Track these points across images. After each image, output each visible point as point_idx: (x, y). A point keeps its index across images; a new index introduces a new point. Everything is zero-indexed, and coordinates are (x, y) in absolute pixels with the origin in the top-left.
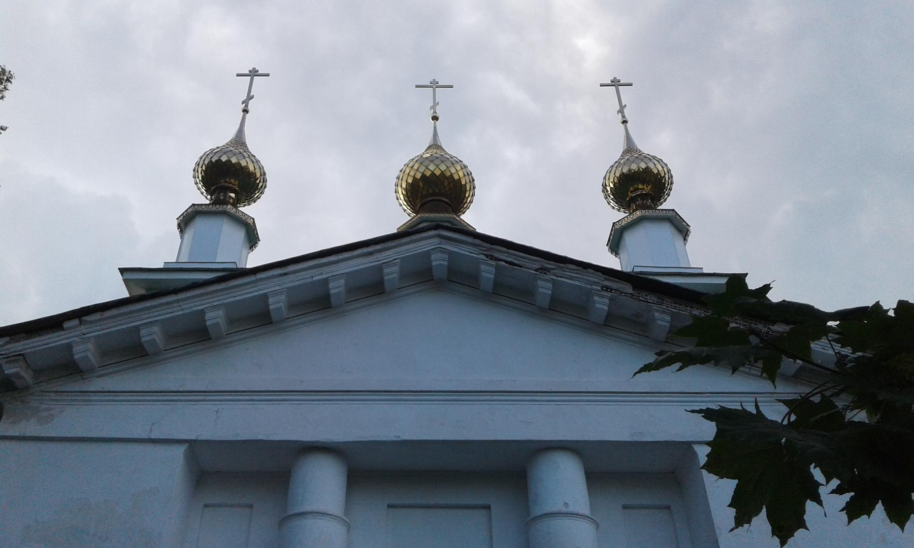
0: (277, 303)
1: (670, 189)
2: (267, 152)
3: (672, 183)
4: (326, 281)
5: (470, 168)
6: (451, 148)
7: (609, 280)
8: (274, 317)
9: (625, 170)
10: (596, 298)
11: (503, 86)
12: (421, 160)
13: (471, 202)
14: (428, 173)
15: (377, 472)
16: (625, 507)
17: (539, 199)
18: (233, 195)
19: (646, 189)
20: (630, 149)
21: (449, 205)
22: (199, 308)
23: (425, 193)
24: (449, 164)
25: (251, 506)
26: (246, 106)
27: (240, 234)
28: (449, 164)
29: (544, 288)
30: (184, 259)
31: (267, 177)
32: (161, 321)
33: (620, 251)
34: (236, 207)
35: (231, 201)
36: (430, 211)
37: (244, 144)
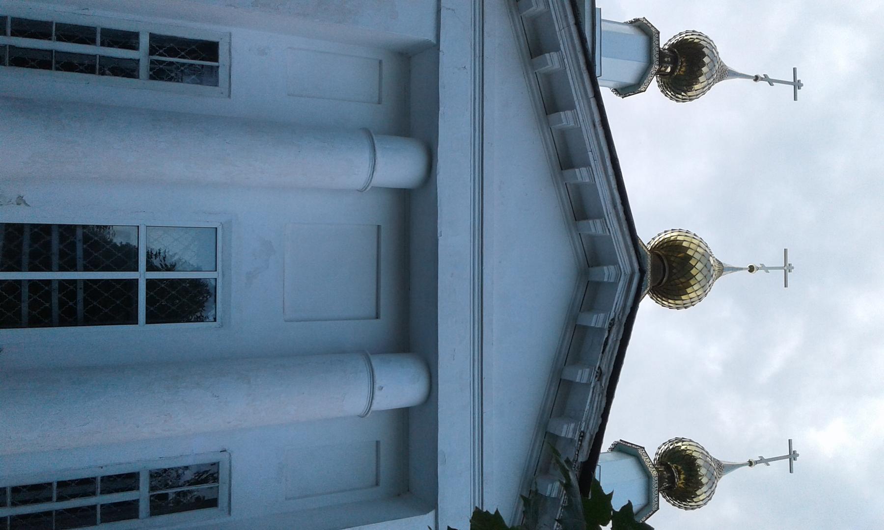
0: (566, 119)
1: (679, 507)
2: (713, 102)
3: (686, 509)
4: (587, 164)
5: (698, 305)
6: (719, 285)
7: (591, 439)
8: (553, 116)
9: (699, 462)
10: (572, 425)
11: (785, 346)
12: (706, 255)
13: (663, 305)
14: (692, 262)
15: (409, 216)
16: (378, 443)
17: (669, 377)
18: (669, 70)
19: (680, 482)
20: (722, 468)
21: (660, 283)
22: (562, 46)
23: (672, 259)
24: (702, 283)
25: (379, 102)
26: (762, 79)
27: (629, 78)
28: (702, 283)
29: (582, 375)
30: (605, 26)
31: (689, 103)
32: (549, 11)
33: (615, 453)
34: (656, 74)
35: (663, 69)
36: (653, 265)
37: (721, 78)
